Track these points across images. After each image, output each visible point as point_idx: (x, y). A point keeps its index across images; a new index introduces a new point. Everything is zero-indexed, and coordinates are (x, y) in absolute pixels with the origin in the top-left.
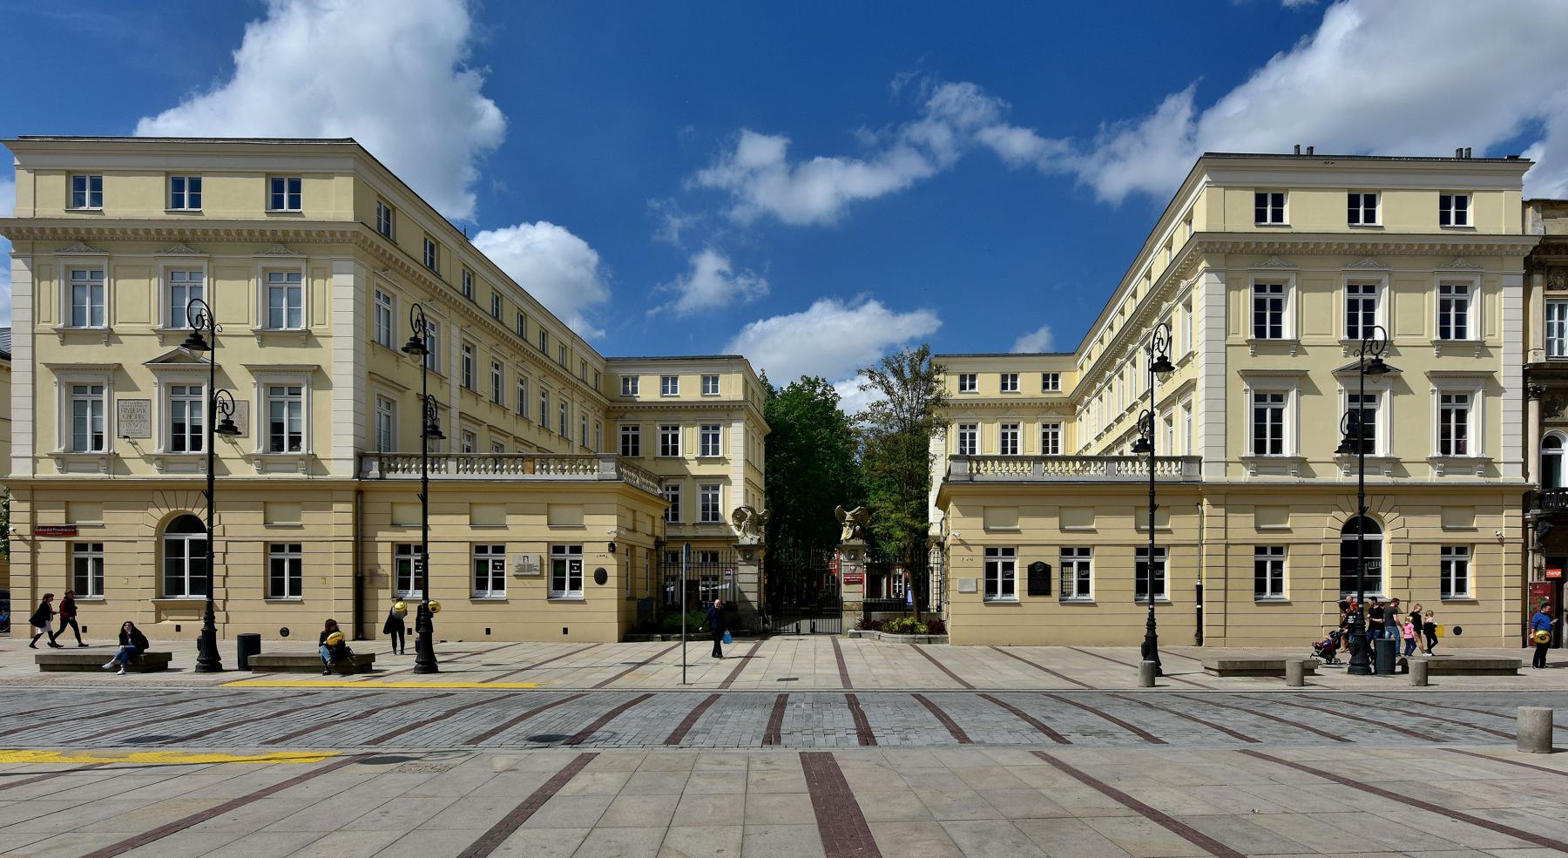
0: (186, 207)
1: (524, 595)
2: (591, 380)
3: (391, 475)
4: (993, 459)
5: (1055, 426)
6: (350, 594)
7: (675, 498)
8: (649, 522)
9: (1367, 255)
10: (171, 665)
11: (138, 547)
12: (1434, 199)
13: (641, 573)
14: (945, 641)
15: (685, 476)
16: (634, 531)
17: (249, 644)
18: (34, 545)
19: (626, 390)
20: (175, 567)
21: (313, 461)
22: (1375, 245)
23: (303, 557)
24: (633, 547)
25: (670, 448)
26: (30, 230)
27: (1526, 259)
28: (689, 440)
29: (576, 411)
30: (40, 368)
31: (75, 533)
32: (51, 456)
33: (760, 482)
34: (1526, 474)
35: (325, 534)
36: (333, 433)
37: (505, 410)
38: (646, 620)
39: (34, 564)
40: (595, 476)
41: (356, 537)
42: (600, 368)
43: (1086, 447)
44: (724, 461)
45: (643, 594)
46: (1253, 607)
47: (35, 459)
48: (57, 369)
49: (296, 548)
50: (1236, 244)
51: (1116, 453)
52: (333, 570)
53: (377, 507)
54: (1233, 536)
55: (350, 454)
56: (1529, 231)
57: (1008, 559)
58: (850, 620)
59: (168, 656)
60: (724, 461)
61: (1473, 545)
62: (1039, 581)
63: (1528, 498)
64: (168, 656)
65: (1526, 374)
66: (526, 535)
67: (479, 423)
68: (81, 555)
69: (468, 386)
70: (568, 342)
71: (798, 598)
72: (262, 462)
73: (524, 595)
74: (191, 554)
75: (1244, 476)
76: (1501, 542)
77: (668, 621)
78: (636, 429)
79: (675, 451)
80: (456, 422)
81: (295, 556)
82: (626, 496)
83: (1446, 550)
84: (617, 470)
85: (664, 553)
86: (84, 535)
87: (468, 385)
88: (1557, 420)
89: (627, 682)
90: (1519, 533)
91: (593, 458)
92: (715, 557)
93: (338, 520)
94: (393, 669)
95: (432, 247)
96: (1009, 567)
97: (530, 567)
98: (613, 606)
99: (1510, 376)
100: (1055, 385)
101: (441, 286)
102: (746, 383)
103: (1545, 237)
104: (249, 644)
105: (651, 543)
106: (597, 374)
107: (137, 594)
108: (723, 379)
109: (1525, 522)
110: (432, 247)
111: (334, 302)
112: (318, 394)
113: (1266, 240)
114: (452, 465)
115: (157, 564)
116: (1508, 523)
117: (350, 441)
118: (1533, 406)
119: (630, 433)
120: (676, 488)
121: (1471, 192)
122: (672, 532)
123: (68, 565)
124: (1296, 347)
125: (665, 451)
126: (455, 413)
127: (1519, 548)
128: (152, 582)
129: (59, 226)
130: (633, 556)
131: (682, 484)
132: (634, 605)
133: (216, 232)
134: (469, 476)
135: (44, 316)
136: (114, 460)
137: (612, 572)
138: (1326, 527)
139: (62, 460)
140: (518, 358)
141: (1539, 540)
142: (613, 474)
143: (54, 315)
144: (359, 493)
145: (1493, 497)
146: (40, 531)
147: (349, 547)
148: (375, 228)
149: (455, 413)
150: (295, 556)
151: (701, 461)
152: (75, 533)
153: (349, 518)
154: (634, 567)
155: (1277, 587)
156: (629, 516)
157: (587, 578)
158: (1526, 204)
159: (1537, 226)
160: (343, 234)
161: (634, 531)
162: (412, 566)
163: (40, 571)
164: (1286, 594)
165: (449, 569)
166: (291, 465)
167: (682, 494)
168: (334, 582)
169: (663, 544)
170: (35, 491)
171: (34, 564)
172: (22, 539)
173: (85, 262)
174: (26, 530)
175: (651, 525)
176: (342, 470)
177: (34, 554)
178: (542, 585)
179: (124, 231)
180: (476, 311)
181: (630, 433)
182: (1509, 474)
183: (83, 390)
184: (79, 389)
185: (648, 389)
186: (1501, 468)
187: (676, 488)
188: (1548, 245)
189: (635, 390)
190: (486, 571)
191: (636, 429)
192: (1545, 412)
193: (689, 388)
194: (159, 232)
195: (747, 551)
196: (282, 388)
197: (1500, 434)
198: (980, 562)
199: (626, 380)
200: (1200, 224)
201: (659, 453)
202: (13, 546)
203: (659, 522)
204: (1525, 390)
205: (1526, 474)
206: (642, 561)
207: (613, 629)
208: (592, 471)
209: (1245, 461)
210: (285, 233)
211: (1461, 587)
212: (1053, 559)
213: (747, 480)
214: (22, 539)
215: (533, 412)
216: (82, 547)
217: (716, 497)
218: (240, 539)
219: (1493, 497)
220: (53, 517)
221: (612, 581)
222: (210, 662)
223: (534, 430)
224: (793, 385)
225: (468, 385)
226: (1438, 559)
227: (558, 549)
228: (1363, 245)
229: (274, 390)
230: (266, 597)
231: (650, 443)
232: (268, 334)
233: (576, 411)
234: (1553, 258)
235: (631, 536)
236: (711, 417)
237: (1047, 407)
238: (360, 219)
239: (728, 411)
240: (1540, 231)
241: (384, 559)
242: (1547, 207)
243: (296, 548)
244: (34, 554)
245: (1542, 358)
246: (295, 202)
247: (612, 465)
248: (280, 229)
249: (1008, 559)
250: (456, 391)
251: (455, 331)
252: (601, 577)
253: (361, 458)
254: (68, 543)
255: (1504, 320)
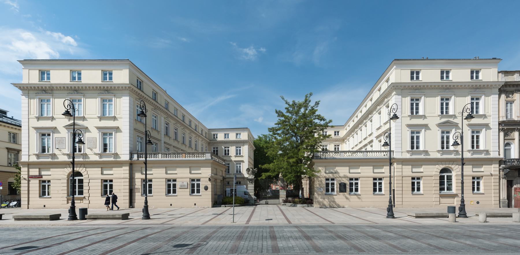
0: (77, 80)
1: (183, 194)
2: (204, 135)
3: (140, 159)
4: (332, 152)
5: (338, 146)
6: (128, 194)
7: (229, 167)
8: (221, 172)
9: (447, 89)
10: (60, 218)
11: (62, 181)
12: (469, 72)
13: (218, 187)
14: (312, 206)
15: (231, 161)
16: (216, 174)
17: (386, 144)
18: (29, 181)
19: (214, 138)
20: (74, 187)
21: (116, 155)
22: (450, 86)
23: (113, 183)
24: (216, 179)
25: (227, 153)
26: (27, 87)
27: (499, 89)
28: (232, 150)
29: (200, 143)
30: (30, 128)
31: (42, 177)
32: (34, 154)
33: (253, 162)
34: (499, 155)
35: (120, 176)
36: (122, 145)
37: (178, 142)
38: (220, 200)
39: (28, 187)
40: (204, 158)
41: (130, 177)
42: (207, 132)
43: (352, 148)
44: (242, 156)
45: (219, 193)
46: (411, 195)
47: (29, 156)
48: (36, 129)
49: (111, 181)
50: (405, 86)
51: (364, 150)
52: (123, 187)
53: (135, 167)
54: (404, 174)
55: (128, 152)
56: (500, 80)
57: (380, 181)
58: (281, 200)
59: (60, 215)
60: (242, 156)
61: (482, 176)
62: (343, 188)
63: (501, 162)
64: (60, 215)
65: (499, 124)
66: (183, 175)
67: (170, 145)
68: (44, 184)
69: (167, 134)
70: (197, 124)
71: (263, 193)
72: (101, 156)
73: (183, 194)
74: (444, 182)
75: (408, 156)
76: (492, 175)
77: (227, 200)
78: (217, 148)
79: (228, 154)
80: (163, 144)
81: (111, 183)
82: (214, 165)
83: (473, 178)
84: (211, 157)
85: (225, 182)
86: (44, 178)
87: (167, 134)
88: (510, 138)
89: (212, 223)
90: (498, 173)
91: (203, 153)
92: (240, 183)
93: (124, 171)
94: (136, 218)
95: (155, 94)
96: (333, 184)
97: (184, 185)
98: (210, 197)
99: (494, 126)
100: (338, 134)
101: (158, 105)
102: (248, 135)
103: (506, 82)
104: (84, 211)
105: (221, 178)
106: (206, 133)
107: (61, 195)
108: (242, 134)
109: (500, 169)
110: (155, 94)
111: (122, 107)
112: (118, 134)
113: (415, 85)
114: (160, 155)
115: (68, 186)
116: (494, 169)
117: (128, 149)
118: (502, 134)
119: (216, 149)
120: (228, 164)
121: (481, 69)
122: (227, 176)
123: (102, 186)
124: (424, 117)
125: (225, 154)
126: (163, 142)
127: (498, 177)
128: (66, 192)
129: (36, 86)
130: (216, 182)
131: (230, 163)
132: (217, 196)
133: (86, 87)
134: (165, 159)
135: (32, 113)
136: (54, 156)
137: (210, 187)
138: (435, 170)
139: (38, 156)
140: (182, 127)
141: (505, 175)
142: (210, 158)
143: (35, 112)
144: (131, 164)
145: (490, 161)
146: (30, 177)
147: (128, 180)
148: (136, 86)
149: (163, 142)
150: (111, 183)
151: (236, 156)
152: (42, 177)
153: (128, 172)
154: (216, 185)
155: (419, 189)
156: (215, 170)
157: (202, 189)
158: (499, 72)
159: (503, 79)
160: (125, 87)
161: (216, 174)
162: (147, 187)
163: (30, 189)
164: (421, 191)
165: (159, 186)
166: (109, 156)
167: (230, 166)
168: (123, 191)
169: (225, 178)
170: (29, 165)
171: (28, 187)
172: (25, 179)
173: (45, 97)
174: (26, 177)
175: (221, 172)
176: (125, 157)
177: (29, 184)
178: (188, 191)
179: (57, 87)
180: (169, 113)
181: (216, 149)
182: (494, 155)
183: (44, 134)
184: (44, 135)
185: (221, 137)
186: (491, 153)
187: (228, 164)
188: (507, 85)
189: (217, 137)
190: (171, 188)
191: (217, 148)
192: (506, 135)
193: (232, 137)
194: (68, 87)
195: (250, 180)
196: (106, 133)
197: (491, 142)
198: (371, 182)
199: (214, 135)
200: (392, 80)
201: (224, 155)
202: (22, 182)
203: (224, 172)
204: (499, 129)
205: (499, 155)
206: (219, 183)
207: (210, 204)
208: (203, 157)
209: (408, 152)
210: (107, 87)
211: (478, 189)
212: (348, 182)
213: (249, 162)
214: (25, 179)
215: (187, 143)
216: (44, 181)
217: (240, 167)
218: (92, 178)
219: (490, 161)
220: (34, 172)
221: (210, 189)
222: (73, 217)
223: (187, 148)
224: (259, 137)
225: (167, 134)
226: (471, 181)
227: (193, 180)
228: (446, 86)
229: (105, 134)
230: (102, 196)
231: (221, 153)
232: (102, 118)
233: (200, 143)
234: (508, 89)
235: (216, 176)
236: (238, 143)
237: (336, 140)
238: (131, 83)
239: (243, 142)
240: (504, 80)
241: (138, 184)
242: (506, 73)
243: (111, 181)
244: (29, 184)
245: (505, 119)
246: (111, 78)
247: (209, 155)
248: (106, 86)
249: (380, 181)
250: (163, 136)
251: (163, 118)
252: (206, 188)
253: (131, 155)
254: (40, 180)
255: (491, 107)
